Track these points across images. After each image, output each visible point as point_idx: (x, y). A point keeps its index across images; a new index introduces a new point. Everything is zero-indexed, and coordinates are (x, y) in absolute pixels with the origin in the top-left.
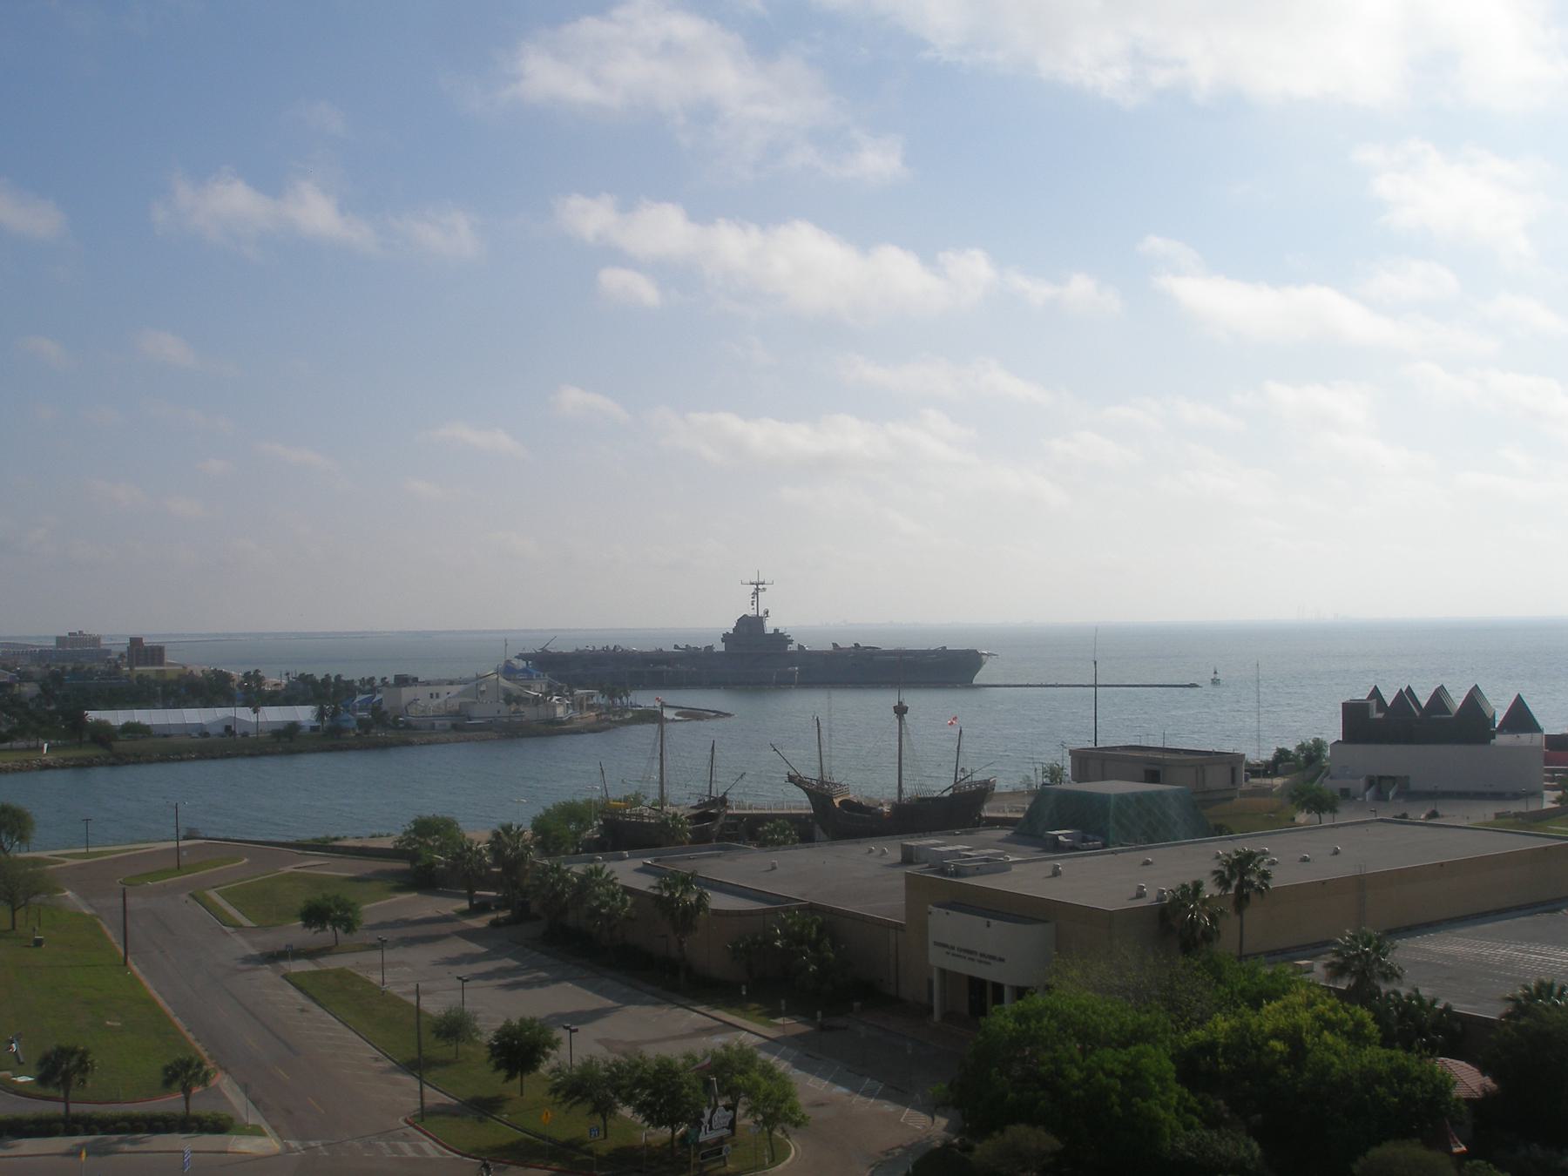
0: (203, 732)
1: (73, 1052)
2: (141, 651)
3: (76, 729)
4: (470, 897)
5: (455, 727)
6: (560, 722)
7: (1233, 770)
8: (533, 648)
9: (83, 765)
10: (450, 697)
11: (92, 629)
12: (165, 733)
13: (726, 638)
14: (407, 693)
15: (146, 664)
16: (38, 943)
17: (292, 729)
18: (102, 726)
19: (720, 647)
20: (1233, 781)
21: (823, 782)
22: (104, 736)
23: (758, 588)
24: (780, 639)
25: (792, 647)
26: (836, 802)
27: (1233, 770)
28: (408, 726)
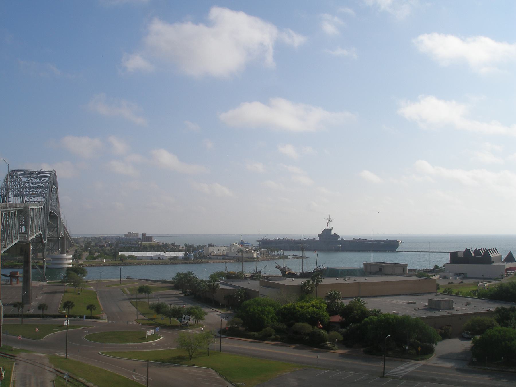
0: (151, 258)
1: (70, 302)
2: (145, 237)
3: (115, 255)
4: (183, 291)
5: (223, 259)
6: (255, 258)
7: (404, 269)
8: (261, 238)
9: (115, 265)
10: (224, 250)
11: (135, 232)
12: (141, 258)
13: (319, 236)
14: (211, 249)
15: (147, 241)
16: (79, 294)
17: (175, 258)
18: (122, 255)
19: (318, 239)
20: (404, 271)
21: (284, 268)
22: (123, 258)
23: (329, 220)
24: (336, 236)
25: (340, 239)
26: (287, 273)
27: (404, 269)
28: (210, 258)
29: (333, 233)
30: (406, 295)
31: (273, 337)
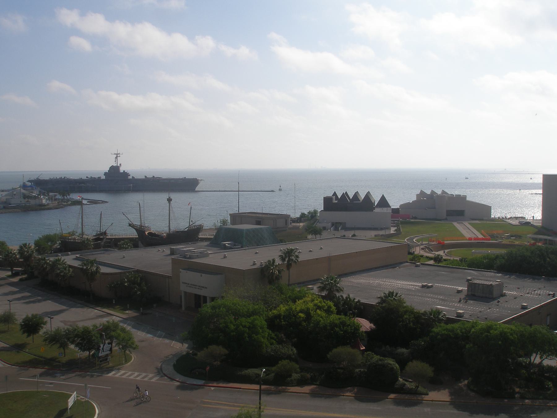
4: (12, 270)
6: (44, 205)
7: (286, 220)
13: (105, 174)
19: (103, 177)
23: (117, 156)
24: (125, 174)
25: (130, 177)
26: (146, 233)
27: (286, 220)
29: (121, 171)
30: (379, 267)
31: (295, 376)
